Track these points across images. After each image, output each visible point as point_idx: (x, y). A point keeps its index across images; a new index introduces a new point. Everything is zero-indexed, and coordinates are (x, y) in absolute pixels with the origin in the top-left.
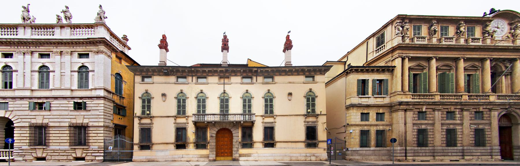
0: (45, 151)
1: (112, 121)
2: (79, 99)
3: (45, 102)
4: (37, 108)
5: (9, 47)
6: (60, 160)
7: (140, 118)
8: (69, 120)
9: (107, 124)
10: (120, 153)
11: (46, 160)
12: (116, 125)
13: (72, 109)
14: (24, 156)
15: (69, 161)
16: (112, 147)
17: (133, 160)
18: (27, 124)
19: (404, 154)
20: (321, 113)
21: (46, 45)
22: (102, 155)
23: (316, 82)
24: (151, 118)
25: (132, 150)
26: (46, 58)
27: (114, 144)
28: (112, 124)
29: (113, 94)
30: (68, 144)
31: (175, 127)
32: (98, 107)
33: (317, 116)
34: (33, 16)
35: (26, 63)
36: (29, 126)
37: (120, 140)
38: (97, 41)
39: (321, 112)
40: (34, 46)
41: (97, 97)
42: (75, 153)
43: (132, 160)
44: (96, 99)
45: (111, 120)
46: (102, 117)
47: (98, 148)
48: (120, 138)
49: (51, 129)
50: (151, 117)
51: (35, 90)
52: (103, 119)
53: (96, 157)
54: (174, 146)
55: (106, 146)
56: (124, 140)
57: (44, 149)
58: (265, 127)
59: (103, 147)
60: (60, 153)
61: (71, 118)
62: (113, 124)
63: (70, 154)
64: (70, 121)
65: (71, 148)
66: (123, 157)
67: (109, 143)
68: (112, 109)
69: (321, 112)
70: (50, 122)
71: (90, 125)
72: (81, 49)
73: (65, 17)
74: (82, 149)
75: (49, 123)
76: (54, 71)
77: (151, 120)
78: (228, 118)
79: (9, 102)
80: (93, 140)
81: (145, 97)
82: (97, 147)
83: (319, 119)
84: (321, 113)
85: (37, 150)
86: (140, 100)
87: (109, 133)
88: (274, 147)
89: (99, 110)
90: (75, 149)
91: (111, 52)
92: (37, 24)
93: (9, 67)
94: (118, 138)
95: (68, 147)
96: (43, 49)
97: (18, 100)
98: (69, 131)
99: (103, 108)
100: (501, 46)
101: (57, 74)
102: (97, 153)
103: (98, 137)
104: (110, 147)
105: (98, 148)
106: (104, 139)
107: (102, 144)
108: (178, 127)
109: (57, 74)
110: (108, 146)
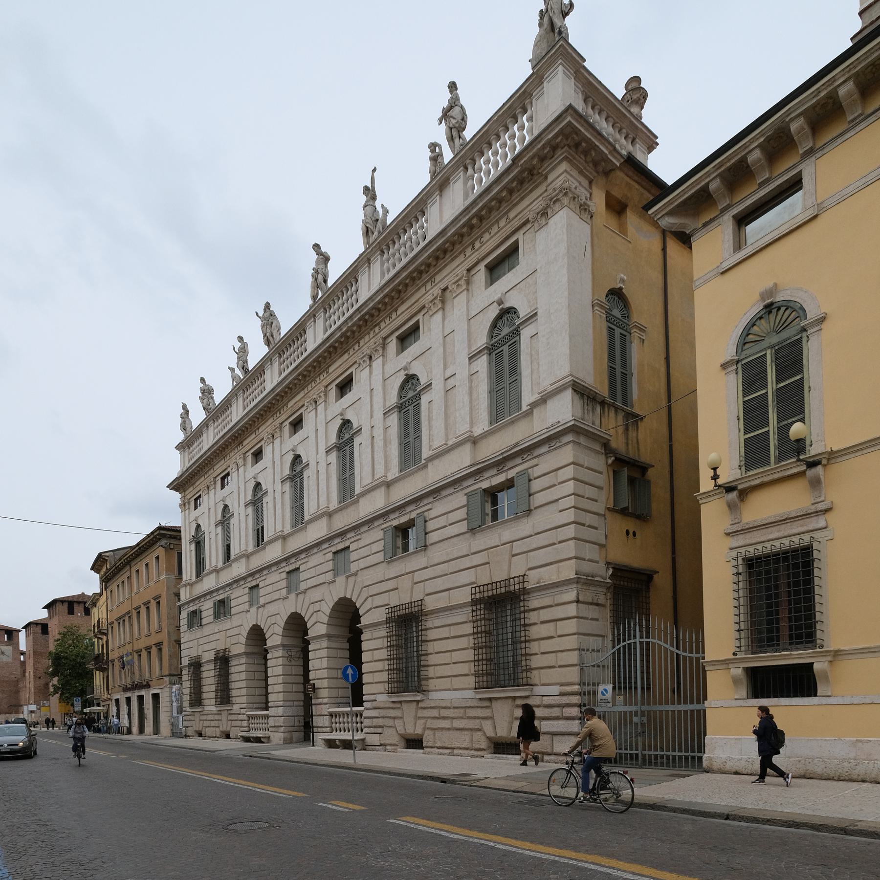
0: (421, 713)
1: (604, 550)
2: (494, 471)
3: (413, 520)
4: (399, 548)
6: (453, 748)
7: (734, 495)
8: (466, 577)
9: (587, 567)
10: (645, 719)
11: (421, 747)
12: (620, 572)
14: (380, 730)
15: (476, 753)
16: (610, 687)
17: (705, 764)
24: (811, 473)
25: (698, 702)
26: (411, 344)
27: (614, 671)
28: (602, 564)
29: (603, 403)
30: (471, 681)
31: (734, 554)
32: (554, 485)
34: (383, 206)
35: (375, 392)
36: (577, 581)
37: (641, 643)
38: (497, 193)
39: (715, 469)
40: (391, 313)
41: (549, 440)
43: (700, 758)
44: (365, 528)
45: (602, 546)
46: (571, 531)
47: (562, 694)
48: (641, 637)
49: (437, 623)
50: (813, 464)
51: (289, 535)
52: (572, 543)
53: (555, 738)
54: (736, 681)
55: (589, 684)
57: (418, 702)
59: (576, 688)
60: (453, 718)
62: (608, 564)
64: (473, 580)
65: (393, 702)
66: (644, 745)
67: (594, 666)
68: (600, 488)
69: (715, 469)
70: (427, 595)
71: (532, 582)
72: (285, 416)
73: (365, 229)
74: (510, 701)
75: (426, 598)
77: (816, 484)
79: (351, 543)
80: (454, 663)
81: (757, 347)
82: (556, 690)
83: (832, 494)
85: (405, 706)
86: (733, 376)
87: (596, 616)
88: (816, 695)
89: (557, 500)
90: (490, 699)
91: (590, 183)
92: (254, 367)
94: (635, 637)
95: (470, 694)
97: (450, 494)
99: (570, 487)
101: (438, 387)
102: (557, 718)
103: (557, 639)
104: (601, 688)
105: (562, 694)
106: (580, 649)
107: (573, 675)
108: (751, 549)
109: (438, 387)
110: (594, 684)
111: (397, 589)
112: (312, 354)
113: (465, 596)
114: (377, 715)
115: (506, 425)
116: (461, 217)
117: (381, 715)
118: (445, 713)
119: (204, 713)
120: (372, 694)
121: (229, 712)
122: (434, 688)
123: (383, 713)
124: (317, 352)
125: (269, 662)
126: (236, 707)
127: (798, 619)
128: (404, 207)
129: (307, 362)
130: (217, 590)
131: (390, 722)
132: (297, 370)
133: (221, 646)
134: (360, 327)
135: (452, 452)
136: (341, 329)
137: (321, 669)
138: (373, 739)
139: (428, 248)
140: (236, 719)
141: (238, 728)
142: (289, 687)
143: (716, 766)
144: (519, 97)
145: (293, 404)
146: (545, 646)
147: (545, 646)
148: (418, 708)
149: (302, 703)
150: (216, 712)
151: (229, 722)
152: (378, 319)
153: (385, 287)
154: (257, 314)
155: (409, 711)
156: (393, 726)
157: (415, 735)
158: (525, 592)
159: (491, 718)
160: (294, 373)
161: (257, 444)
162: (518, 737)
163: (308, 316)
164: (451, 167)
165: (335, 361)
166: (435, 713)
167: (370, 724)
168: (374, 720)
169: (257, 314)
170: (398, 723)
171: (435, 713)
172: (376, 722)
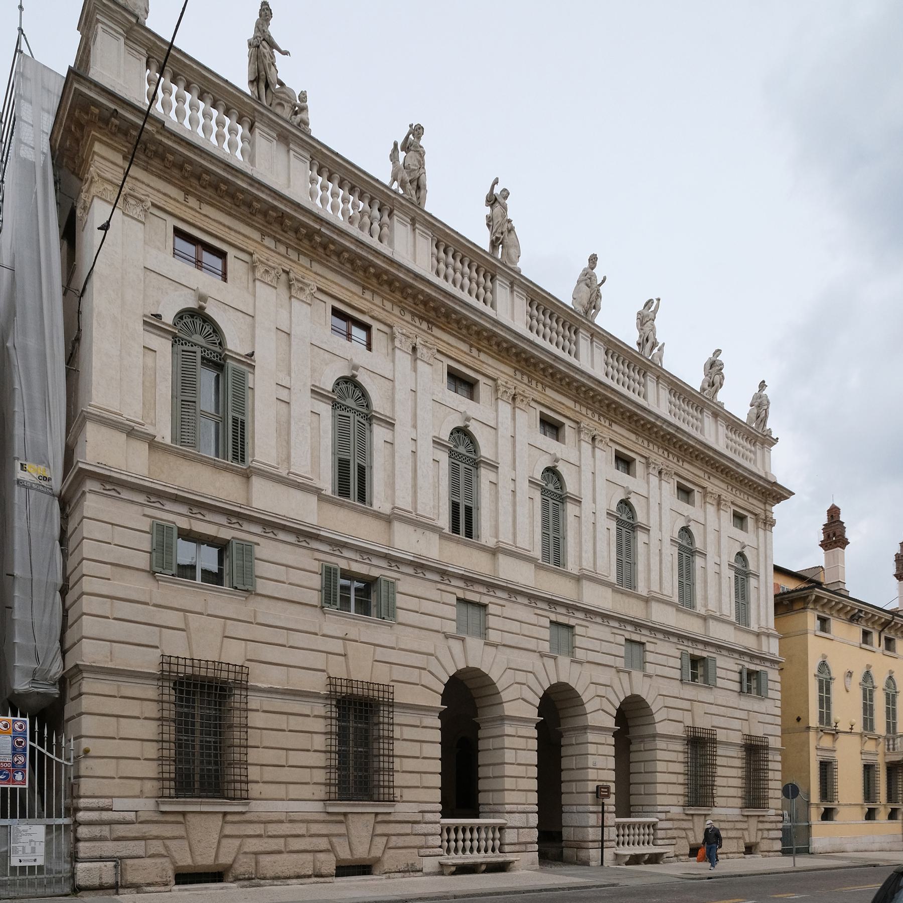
5: (465, 347)
13: (315, 598)
14: (674, 841)
18: (148, 661)
19: (605, 844)
20: (851, 729)
21: (698, 463)
22: (506, 846)
23: (896, 656)
33: (835, 734)
42: (347, 836)
56: (41, 755)
58: (865, 765)
61: (328, 653)
63: (323, 843)
76: (495, 467)
78: (896, 746)
84: (851, 729)
85: (696, 818)
93: (358, 393)
96: (691, 472)
98: (393, 724)
100: (745, 469)
111: (705, 713)
112: (602, 386)
113: (317, 683)
114: (671, 826)
115: (178, 453)
116: (337, 231)
117: (675, 827)
118: (273, 829)
119: (247, 817)
120: (667, 805)
121: (761, 819)
122: (258, 796)
123: (677, 824)
124: (627, 403)
125: (631, 755)
126: (402, 810)
127: (187, 754)
128: (319, 140)
129: (612, 394)
130: (567, 606)
131: (683, 833)
132: (597, 385)
133: (704, 723)
134: (517, 355)
135: (724, 624)
136: (657, 420)
137: (604, 769)
138: (670, 850)
139: (267, 191)
140: (409, 831)
141: (416, 851)
142: (650, 789)
143: (820, 850)
144: (533, 289)
145: (559, 400)
146: (409, 764)
147: (409, 764)
148: (225, 822)
149: (565, 809)
150: (741, 818)
151: (760, 833)
152: (386, 293)
153: (442, 293)
154: (496, 182)
155: (753, 824)
156: (164, 852)
157: (369, 859)
158: (391, 705)
159: (692, 829)
160: (592, 382)
161: (636, 453)
162: (703, 843)
163: (589, 327)
164: (149, 39)
165: (623, 427)
166: (258, 829)
167: (664, 836)
168: (669, 831)
169: (496, 182)
170: (690, 834)
171: (258, 829)
172: (670, 833)
